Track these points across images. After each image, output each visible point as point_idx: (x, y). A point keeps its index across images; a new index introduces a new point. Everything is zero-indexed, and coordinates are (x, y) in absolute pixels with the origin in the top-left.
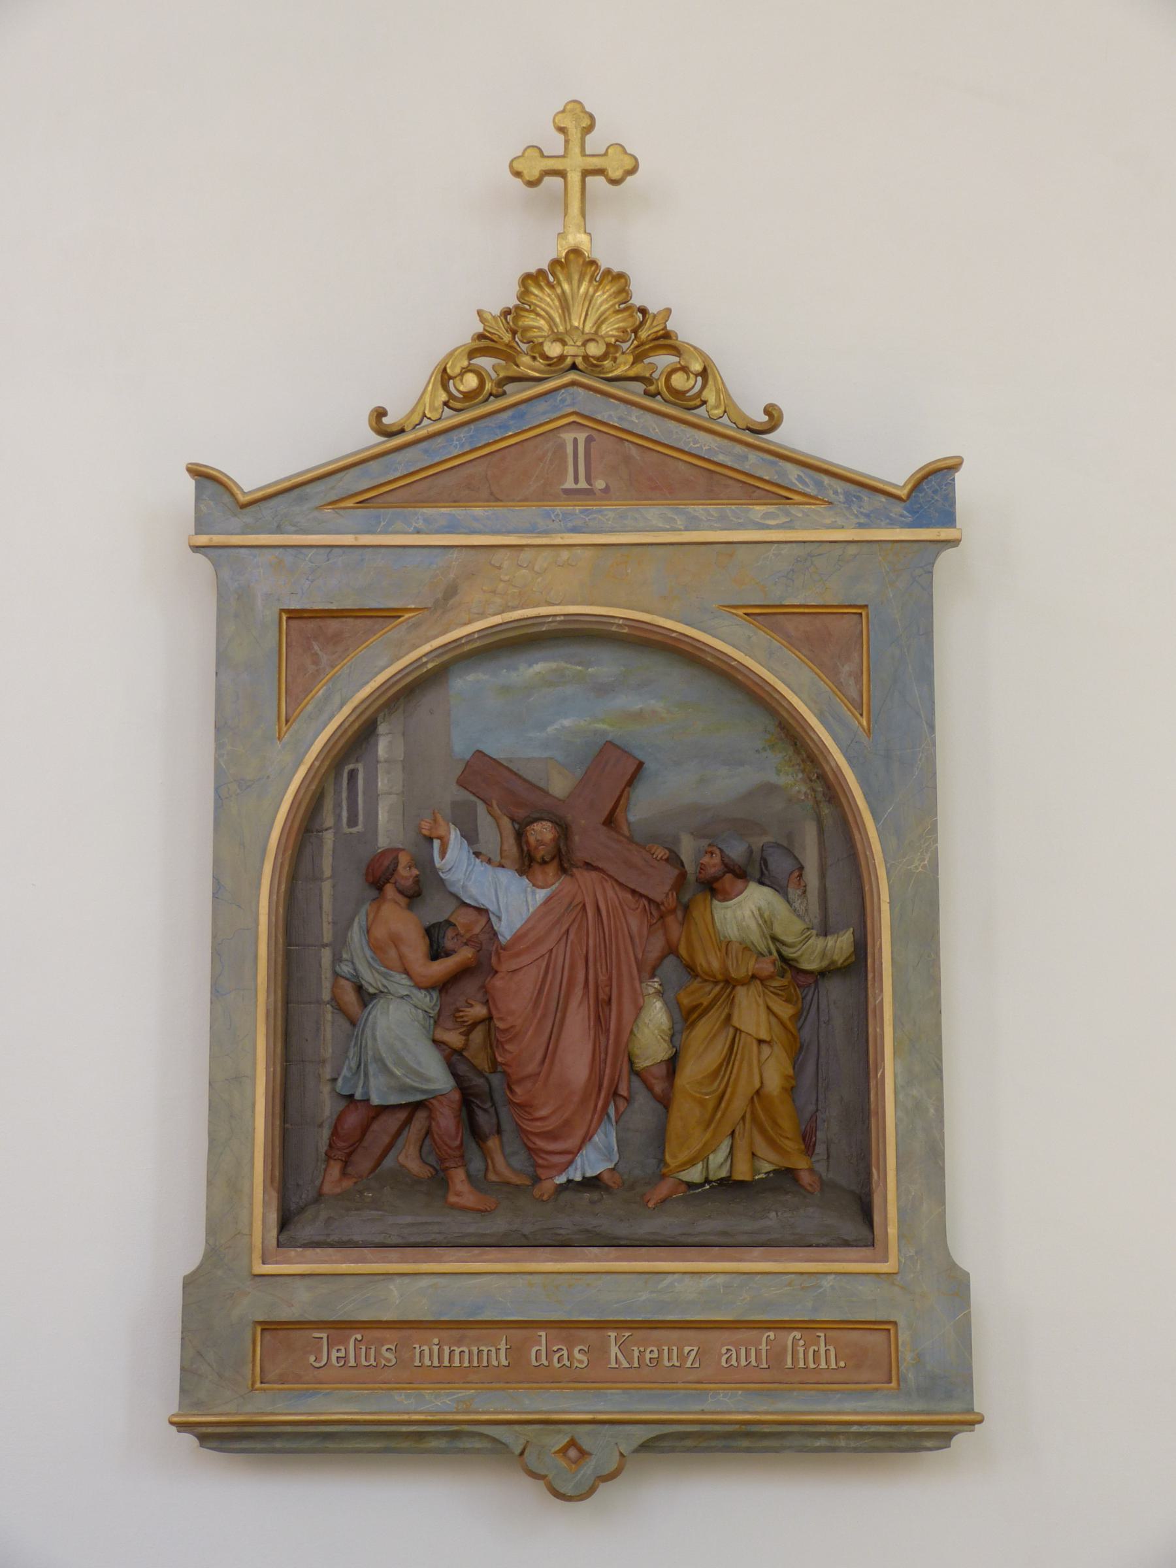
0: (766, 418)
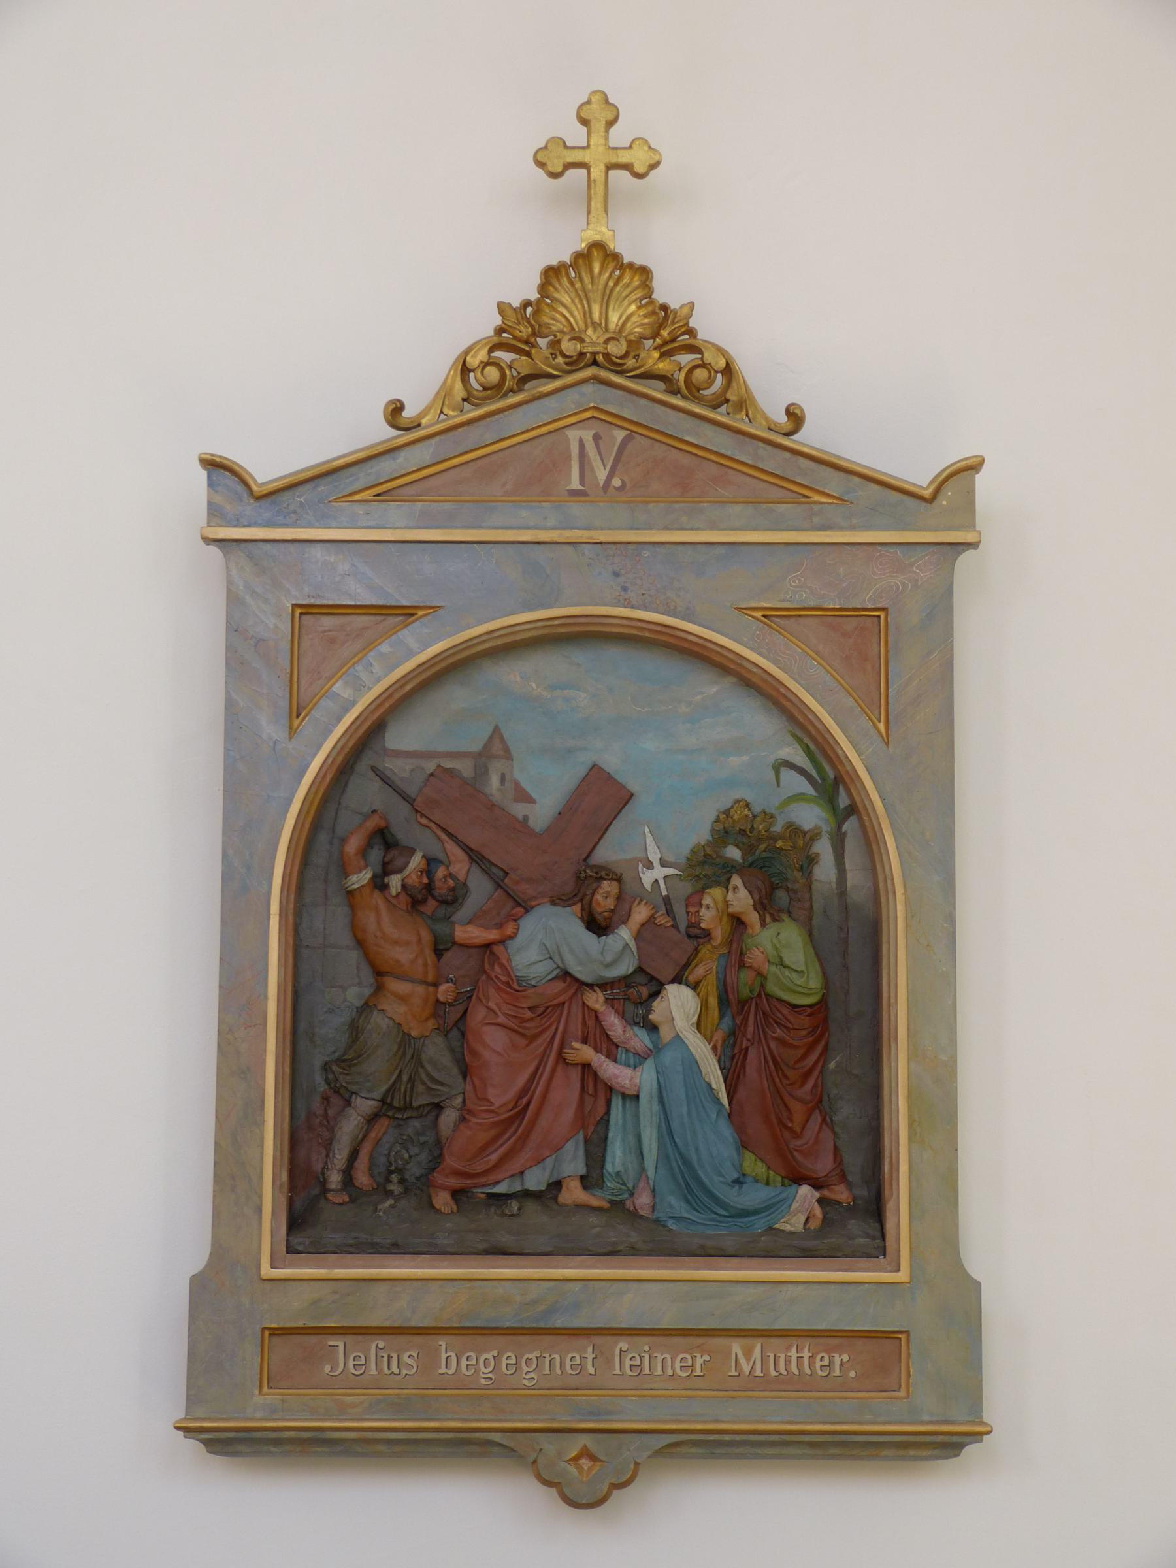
0: (782, 418)
